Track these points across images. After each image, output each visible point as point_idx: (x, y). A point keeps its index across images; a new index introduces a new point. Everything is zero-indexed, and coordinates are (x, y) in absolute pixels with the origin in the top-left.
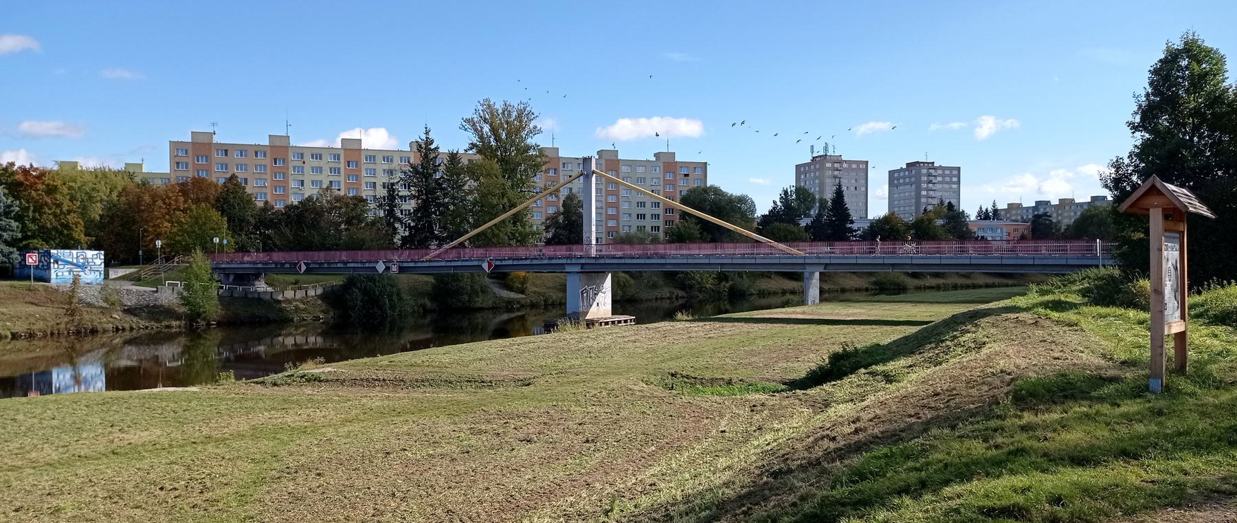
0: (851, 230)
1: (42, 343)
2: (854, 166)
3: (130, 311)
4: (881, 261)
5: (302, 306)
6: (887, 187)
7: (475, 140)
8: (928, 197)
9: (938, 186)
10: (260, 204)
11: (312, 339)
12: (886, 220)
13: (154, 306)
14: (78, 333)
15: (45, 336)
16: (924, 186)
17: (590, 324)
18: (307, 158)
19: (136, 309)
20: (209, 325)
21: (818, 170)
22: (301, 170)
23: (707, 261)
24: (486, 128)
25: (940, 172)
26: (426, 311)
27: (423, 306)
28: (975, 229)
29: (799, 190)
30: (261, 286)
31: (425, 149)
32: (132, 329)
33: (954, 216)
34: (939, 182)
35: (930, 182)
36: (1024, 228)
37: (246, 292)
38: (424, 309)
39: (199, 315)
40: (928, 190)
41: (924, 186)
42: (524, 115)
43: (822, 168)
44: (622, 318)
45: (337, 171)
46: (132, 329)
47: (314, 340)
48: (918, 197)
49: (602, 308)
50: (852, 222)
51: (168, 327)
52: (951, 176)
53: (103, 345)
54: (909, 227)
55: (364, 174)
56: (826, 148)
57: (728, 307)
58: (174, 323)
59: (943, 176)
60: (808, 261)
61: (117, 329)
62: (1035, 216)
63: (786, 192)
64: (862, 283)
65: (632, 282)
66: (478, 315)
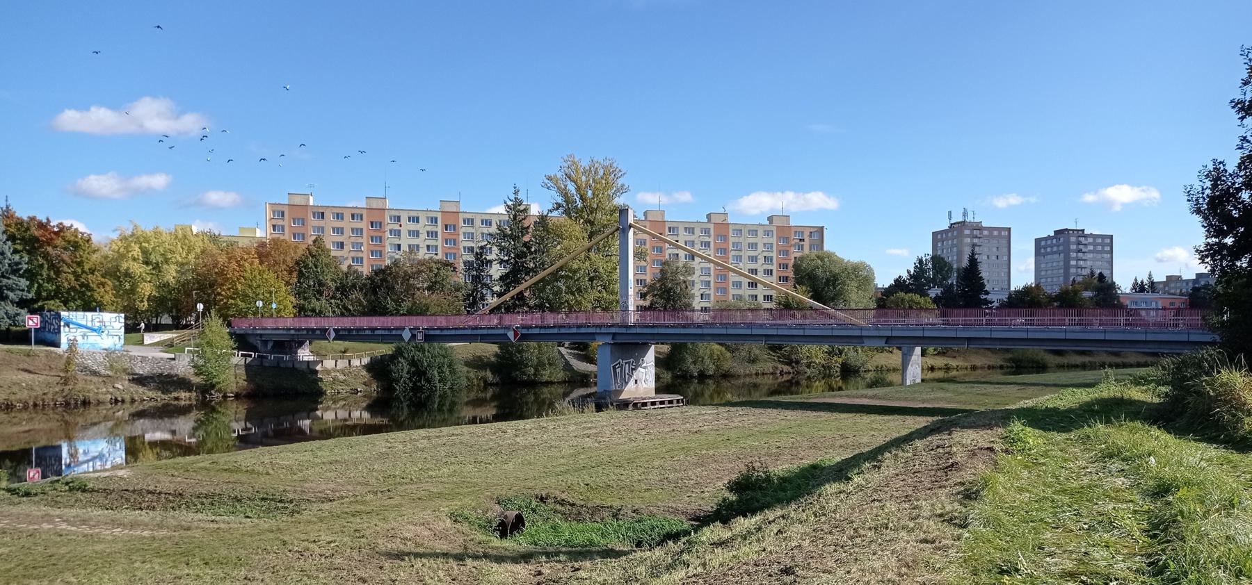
0: (987, 302)
1: (25, 415)
2: (996, 233)
3: (140, 380)
4: (1101, 337)
5: (341, 377)
6: (1032, 260)
7: (560, 200)
8: (1077, 267)
9: (1090, 256)
10: (344, 268)
11: (356, 414)
12: (1027, 291)
13: (169, 376)
14: (67, 404)
15: (25, 408)
16: (1073, 255)
17: (624, 405)
18: (404, 220)
19: (147, 378)
20: (225, 397)
21: (957, 237)
22: (397, 233)
23: (749, 332)
24: (571, 188)
25: (1090, 240)
26: (487, 384)
27: (485, 380)
28: (1128, 302)
29: (936, 259)
30: (304, 354)
31: (517, 211)
32: (133, 401)
33: (1104, 289)
34: (1090, 252)
35: (1080, 251)
36: (1180, 301)
37: (279, 360)
38: (485, 382)
39: (213, 386)
40: (1078, 259)
41: (1073, 255)
42: (610, 173)
43: (961, 236)
44: (667, 397)
45: (433, 234)
46: (133, 401)
47: (360, 415)
48: (1067, 267)
49: (642, 385)
50: (987, 293)
51: (177, 399)
52: (1103, 245)
53: (106, 418)
54: (1051, 299)
55: (462, 237)
56: (965, 214)
57: (840, 384)
58: (183, 395)
59: (1095, 244)
60: (865, 333)
61: (116, 401)
62: (1194, 289)
63: (921, 261)
64: (996, 360)
65: (728, 355)
66: (545, 390)
